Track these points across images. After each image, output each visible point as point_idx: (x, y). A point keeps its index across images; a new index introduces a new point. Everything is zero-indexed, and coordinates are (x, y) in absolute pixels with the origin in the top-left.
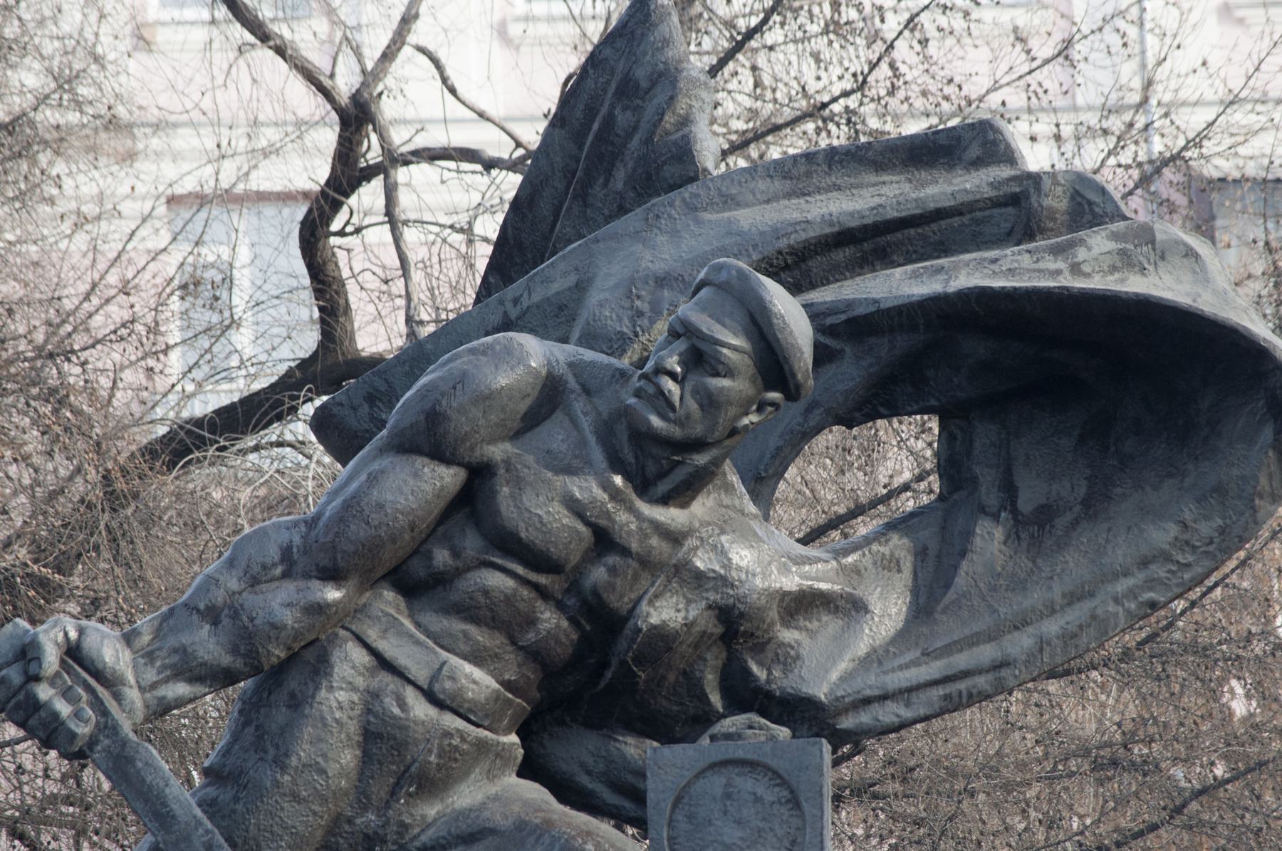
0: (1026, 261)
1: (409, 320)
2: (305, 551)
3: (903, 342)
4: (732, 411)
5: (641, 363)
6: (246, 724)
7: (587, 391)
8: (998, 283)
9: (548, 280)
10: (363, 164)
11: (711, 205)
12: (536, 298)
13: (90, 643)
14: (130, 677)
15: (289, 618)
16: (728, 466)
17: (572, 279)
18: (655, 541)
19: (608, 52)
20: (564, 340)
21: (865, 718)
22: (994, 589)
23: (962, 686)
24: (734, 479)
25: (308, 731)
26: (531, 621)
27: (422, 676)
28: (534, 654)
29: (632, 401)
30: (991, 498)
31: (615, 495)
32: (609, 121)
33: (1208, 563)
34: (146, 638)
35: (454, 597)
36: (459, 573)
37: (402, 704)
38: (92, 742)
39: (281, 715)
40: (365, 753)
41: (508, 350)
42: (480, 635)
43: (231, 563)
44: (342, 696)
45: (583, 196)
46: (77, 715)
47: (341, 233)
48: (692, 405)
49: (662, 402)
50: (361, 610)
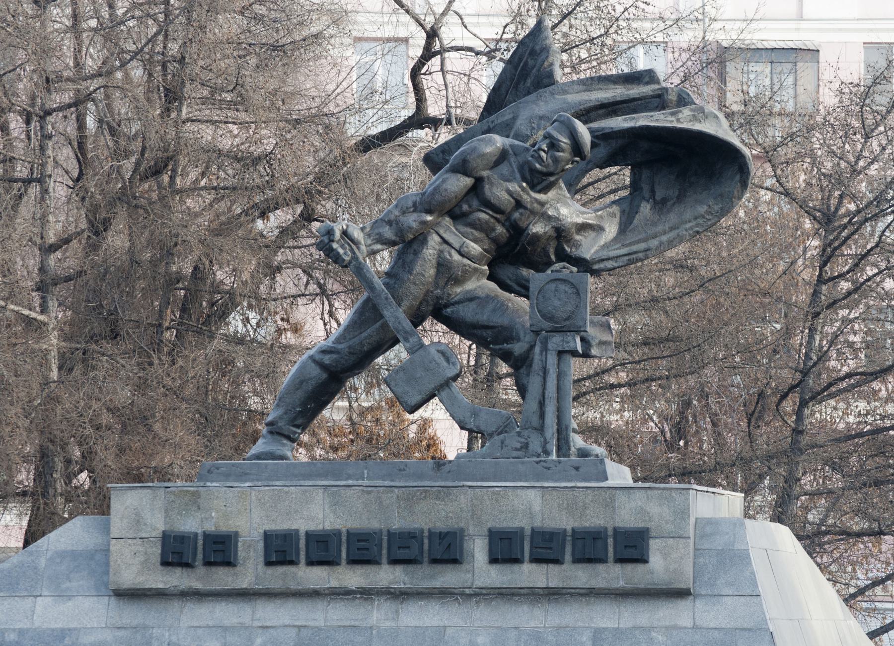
0: (662, 117)
1: (447, 106)
2: (421, 203)
3: (620, 142)
4: (563, 163)
5: (534, 145)
6: (400, 259)
7: (515, 154)
8: (652, 124)
9: (503, 116)
10: (433, 50)
11: (558, 93)
12: (499, 121)
13: (350, 230)
14: (363, 242)
15: (415, 225)
16: (561, 181)
17: (511, 116)
18: (535, 205)
19: (527, 40)
20: (508, 137)
21: (602, 266)
22: (646, 225)
23: (634, 256)
24: (563, 185)
25: (419, 262)
26: (494, 230)
27: (457, 246)
28: (494, 241)
29: (530, 159)
30: (647, 194)
31: (523, 189)
32: (526, 64)
33: (716, 219)
34: (368, 229)
35: (469, 221)
36: (471, 213)
37: (450, 255)
38: (350, 262)
39: (411, 257)
40: (438, 270)
41: (490, 140)
42: (477, 234)
43: (396, 206)
44: (431, 251)
45: (516, 88)
46: (345, 253)
47: (425, 74)
48: (550, 161)
49: (540, 159)
50: (438, 224)
